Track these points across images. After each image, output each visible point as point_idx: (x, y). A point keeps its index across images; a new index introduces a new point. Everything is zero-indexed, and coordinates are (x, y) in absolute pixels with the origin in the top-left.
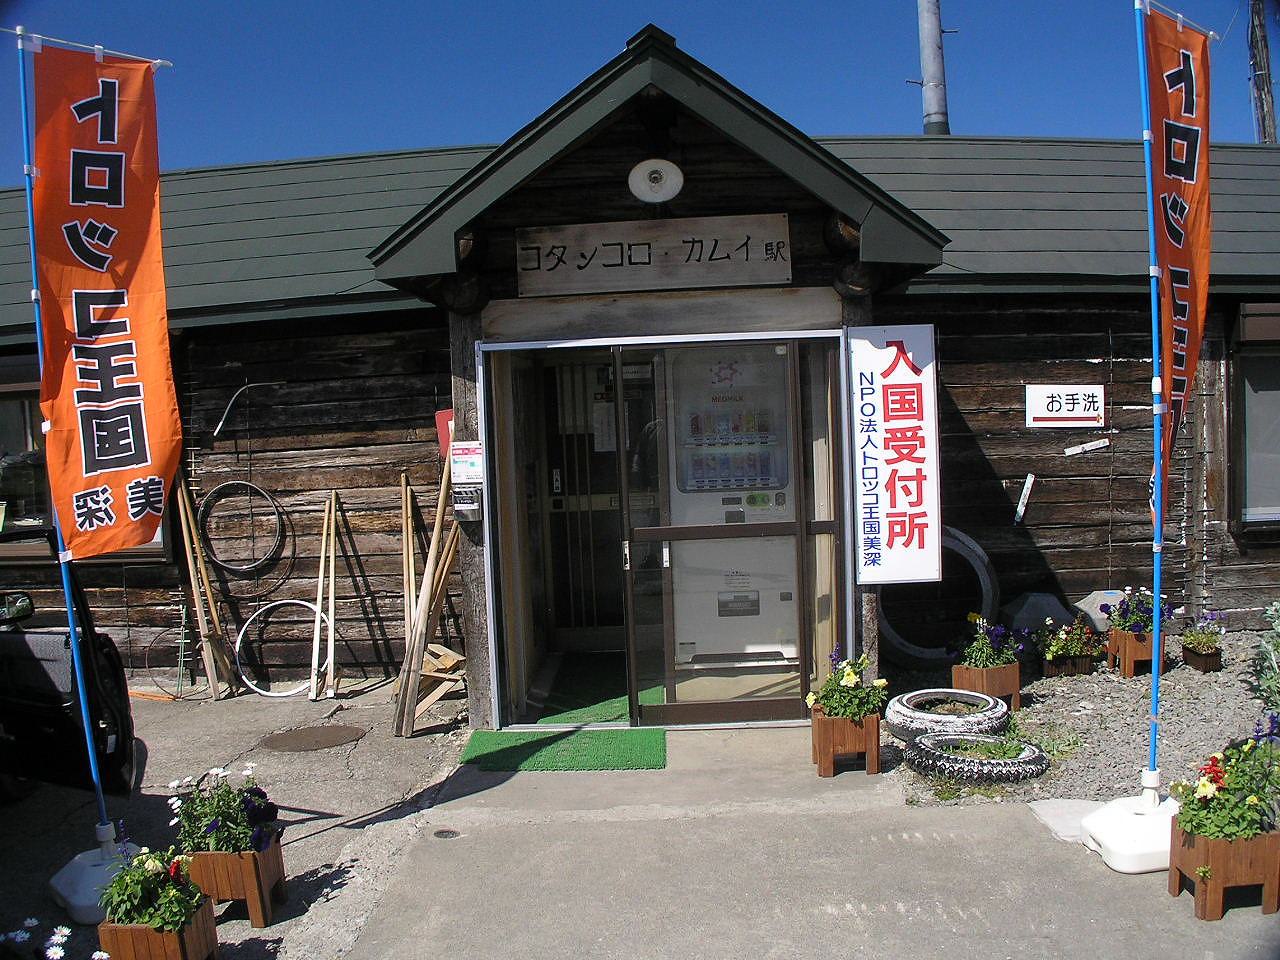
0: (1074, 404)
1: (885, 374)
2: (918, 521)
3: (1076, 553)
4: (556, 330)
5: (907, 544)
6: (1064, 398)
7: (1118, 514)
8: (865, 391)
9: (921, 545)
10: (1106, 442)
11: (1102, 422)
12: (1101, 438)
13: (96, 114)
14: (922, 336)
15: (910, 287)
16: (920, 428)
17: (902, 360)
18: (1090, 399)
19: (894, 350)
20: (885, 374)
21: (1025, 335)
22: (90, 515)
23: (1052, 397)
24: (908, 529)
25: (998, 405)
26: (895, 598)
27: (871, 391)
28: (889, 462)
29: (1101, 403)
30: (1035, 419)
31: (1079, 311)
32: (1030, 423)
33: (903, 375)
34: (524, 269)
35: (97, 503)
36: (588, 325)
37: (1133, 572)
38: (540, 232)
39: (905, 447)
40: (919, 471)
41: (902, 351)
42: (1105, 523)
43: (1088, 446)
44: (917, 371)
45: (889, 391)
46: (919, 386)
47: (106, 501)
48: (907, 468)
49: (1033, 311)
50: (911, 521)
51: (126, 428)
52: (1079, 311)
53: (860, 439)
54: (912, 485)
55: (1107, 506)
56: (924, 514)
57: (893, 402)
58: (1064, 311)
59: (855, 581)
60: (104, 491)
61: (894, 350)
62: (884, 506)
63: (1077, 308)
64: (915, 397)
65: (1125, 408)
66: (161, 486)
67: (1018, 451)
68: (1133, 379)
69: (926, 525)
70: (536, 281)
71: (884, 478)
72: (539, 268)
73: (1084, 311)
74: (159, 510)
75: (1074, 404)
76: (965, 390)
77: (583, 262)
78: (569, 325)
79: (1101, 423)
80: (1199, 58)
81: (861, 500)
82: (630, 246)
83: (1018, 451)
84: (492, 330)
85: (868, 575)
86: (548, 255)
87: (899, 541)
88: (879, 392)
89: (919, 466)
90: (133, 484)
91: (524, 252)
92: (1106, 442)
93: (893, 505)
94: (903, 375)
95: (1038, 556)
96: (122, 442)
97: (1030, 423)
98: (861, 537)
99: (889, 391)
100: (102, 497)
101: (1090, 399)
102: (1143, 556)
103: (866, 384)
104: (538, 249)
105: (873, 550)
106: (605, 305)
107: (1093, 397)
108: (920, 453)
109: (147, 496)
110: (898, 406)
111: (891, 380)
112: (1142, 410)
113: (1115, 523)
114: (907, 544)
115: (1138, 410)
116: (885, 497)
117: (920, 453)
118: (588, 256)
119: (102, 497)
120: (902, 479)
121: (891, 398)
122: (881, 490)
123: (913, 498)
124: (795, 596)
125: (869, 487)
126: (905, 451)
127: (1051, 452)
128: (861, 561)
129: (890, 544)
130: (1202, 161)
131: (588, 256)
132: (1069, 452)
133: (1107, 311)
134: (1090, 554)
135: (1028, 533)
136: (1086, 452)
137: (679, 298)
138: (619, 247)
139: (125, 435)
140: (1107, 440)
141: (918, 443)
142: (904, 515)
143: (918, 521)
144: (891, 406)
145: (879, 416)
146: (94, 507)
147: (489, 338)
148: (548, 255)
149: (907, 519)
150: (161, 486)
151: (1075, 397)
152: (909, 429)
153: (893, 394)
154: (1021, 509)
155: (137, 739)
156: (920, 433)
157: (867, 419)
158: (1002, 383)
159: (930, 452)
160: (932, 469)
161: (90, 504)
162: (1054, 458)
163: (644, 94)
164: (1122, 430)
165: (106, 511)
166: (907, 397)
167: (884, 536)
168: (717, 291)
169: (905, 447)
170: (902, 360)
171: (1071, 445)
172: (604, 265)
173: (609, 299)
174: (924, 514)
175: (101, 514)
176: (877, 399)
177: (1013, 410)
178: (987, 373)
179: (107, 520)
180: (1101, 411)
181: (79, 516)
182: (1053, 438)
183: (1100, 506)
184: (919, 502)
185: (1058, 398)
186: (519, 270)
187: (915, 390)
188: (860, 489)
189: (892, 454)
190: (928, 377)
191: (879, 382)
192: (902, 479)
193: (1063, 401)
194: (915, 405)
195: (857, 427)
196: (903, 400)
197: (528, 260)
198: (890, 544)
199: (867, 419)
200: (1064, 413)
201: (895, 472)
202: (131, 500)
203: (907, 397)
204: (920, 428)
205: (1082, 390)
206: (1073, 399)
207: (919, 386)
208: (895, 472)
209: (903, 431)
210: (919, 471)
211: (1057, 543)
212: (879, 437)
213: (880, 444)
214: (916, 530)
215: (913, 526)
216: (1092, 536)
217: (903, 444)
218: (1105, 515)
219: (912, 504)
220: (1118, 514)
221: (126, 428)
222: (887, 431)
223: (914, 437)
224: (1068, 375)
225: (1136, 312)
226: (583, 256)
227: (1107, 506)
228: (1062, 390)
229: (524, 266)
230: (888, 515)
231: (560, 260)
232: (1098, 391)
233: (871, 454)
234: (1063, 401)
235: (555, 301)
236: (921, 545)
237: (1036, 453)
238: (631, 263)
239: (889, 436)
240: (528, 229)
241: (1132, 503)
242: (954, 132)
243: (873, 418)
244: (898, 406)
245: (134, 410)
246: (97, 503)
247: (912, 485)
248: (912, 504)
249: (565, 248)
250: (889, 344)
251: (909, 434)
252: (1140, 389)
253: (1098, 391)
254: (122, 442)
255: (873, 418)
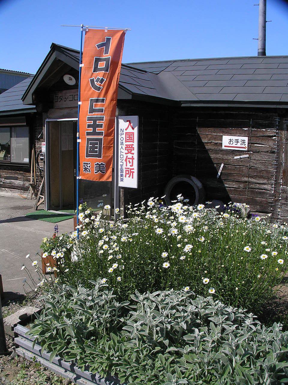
0: (237, 142)
1: (126, 130)
2: (132, 171)
3: (236, 190)
5: (129, 177)
6: (234, 140)
7: (250, 179)
8: (122, 134)
9: (133, 178)
10: (248, 156)
11: (247, 149)
12: (246, 154)
13: (104, 62)
14: (135, 118)
15: (182, 104)
16: (133, 145)
17: (130, 126)
18: (243, 141)
19: (128, 123)
20: (126, 130)
21: (223, 120)
22: (86, 169)
23: (231, 140)
24: (130, 172)
25: (213, 141)
26: (127, 190)
27: (123, 134)
28: (126, 154)
29: (247, 143)
30: (225, 146)
31: (242, 113)
32: (223, 148)
33: (130, 130)
35: (88, 166)
37: (254, 199)
39: (130, 150)
40: (133, 157)
41: (130, 123)
42: (246, 182)
43: (242, 157)
44: (133, 129)
46: (133, 133)
47: (89, 167)
48: (130, 156)
49: (227, 112)
50: (130, 171)
51: (97, 146)
52: (242, 113)
53: (120, 147)
54: (131, 160)
55: (247, 176)
56: (133, 169)
57: (128, 137)
58: (237, 112)
60: (89, 164)
61: (128, 123)
62: (124, 166)
63: (241, 112)
64: (132, 136)
65: (255, 145)
67: (220, 156)
68: (258, 136)
69: (134, 172)
70: (58, 104)
71: (125, 158)
73: (244, 113)
75: (237, 142)
76: (204, 136)
77: (65, 100)
79: (246, 149)
81: (120, 163)
82: (74, 95)
83: (220, 156)
84: (50, 116)
85: (121, 184)
87: (128, 175)
88: (125, 134)
89: (133, 155)
92: (248, 156)
93: (126, 166)
94: (130, 130)
95: (224, 189)
96: (95, 150)
97: (223, 148)
98: (119, 174)
100: (88, 165)
101: (243, 141)
102: (258, 194)
103: (122, 132)
104: (58, 97)
105: (122, 177)
107: (244, 140)
108: (133, 152)
110: (128, 138)
111: (127, 131)
112: (261, 146)
113: (249, 182)
114: (129, 177)
115: (260, 146)
116: (125, 163)
117: (133, 152)
118: (67, 98)
119: (88, 165)
120: (129, 158)
121: (127, 136)
122: (124, 161)
123: (131, 164)
125: (122, 160)
126: (130, 151)
127: (230, 157)
128: (119, 180)
129: (126, 176)
130: (111, 66)
132: (236, 158)
133: (251, 113)
134: (240, 191)
135: (223, 182)
136: (241, 158)
138: (72, 96)
139: (96, 148)
140: (248, 155)
141: (132, 149)
142: (129, 168)
143: (132, 171)
144: (127, 138)
145: (124, 141)
146: (87, 167)
147: (49, 118)
149: (129, 170)
151: (238, 140)
152: (131, 145)
153: (128, 135)
154: (219, 174)
156: (133, 146)
157: (122, 141)
158: (215, 134)
159: (135, 151)
160: (136, 156)
161: (86, 166)
162: (230, 159)
164: (254, 152)
166: (131, 136)
167: (124, 174)
169: (130, 150)
170: (130, 126)
171: (236, 155)
172: (70, 101)
173: (71, 108)
174: (133, 169)
175: (88, 170)
176: (124, 136)
177: (218, 143)
178: (211, 131)
179: (89, 172)
180: (247, 146)
182: (231, 153)
183: (245, 176)
184: (132, 166)
185: (232, 140)
186: (54, 102)
188: (120, 161)
189: (127, 152)
190: (136, 131)
191: (125, 131)
192: (129, 158)
193: (234, 141)
194: (132, 138)
195: (120, 144)
196: (129, 137)
198: (126, 176)
199: (122, 141)
200: (234, 145)
201: (127, 156)
203: (131, 136)
204: (133, 145)
205: (240, 138)
206: (237, 141)
207: (133, 133)
208: (127, 156)
209: (129, 145)
210: (133, 157)
211: (231, 186)
212: (124, 147)
213: (124, 148)
214: (131, 173)
215: (131, 172)
216: (242, 186)
217: (129, 149)
218: (246, 179)
219: (131, 166)
220: (250, 179)
221: (97, 146)
222: (126, 145)
223: (132, 147)
224: (236, 133)
225: (261, 114)
226: (66, 98)
227: (247, 176)
228: (234, 138)
230: (125, 168)
232: (246, 139)
233: (122, 151)
234: (234, 141)
235: (61, 109)
236: (133, 178)
237: (225, 157)
238: (74, 100)
239: (126, 146)
241: (255, 177)
242: (268, 54)
243: (123, 141)
244: (128, 138)
246: (88, 166)
247: (131, 160)
248: (131, 166)
250: (127, 121)
251: (131, 146)
252: (261, 139)
253: (246, 139)
254: (95, 150)
255: (123, 141)
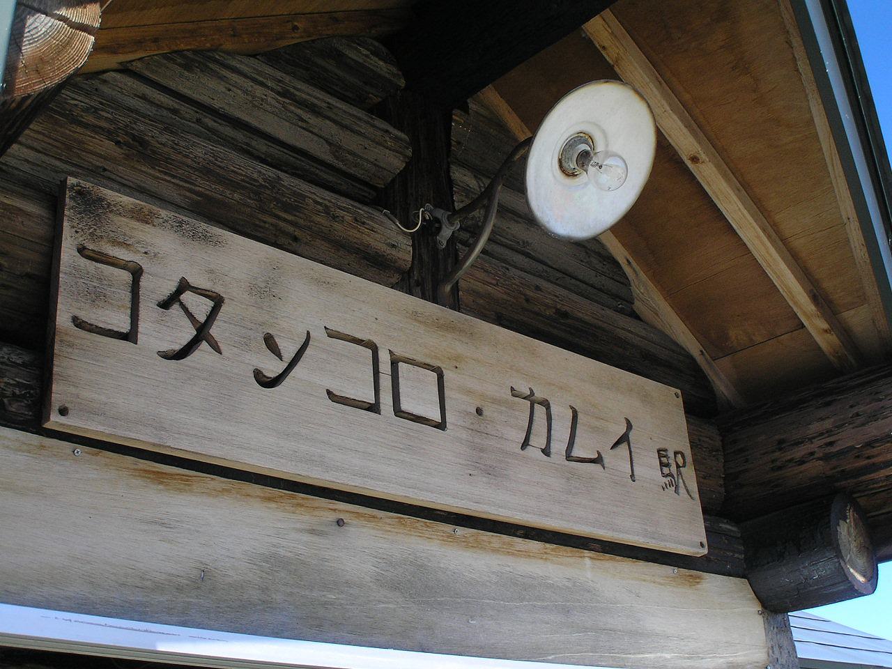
4: (158, 587)
34: (78, 323)
36: (264, 590)
38: (144, 218)
72: (130, 336)
77: (273, 368)
78: (203, 578)
86: (165, 305)
91: (84, 262)
106: (312, 532)
124: (689, 164)
131: (289, 350)
137: (495, 551)
148: (165, 305)
163: (526, 149)
168: (422, 522)
173: (327, 510)
186: (63, 319)
197: (97, 297)
226: (270, 343)
229: (84, 315)
231: (202, 333)
240: (110, 194)
249: (441, 426)
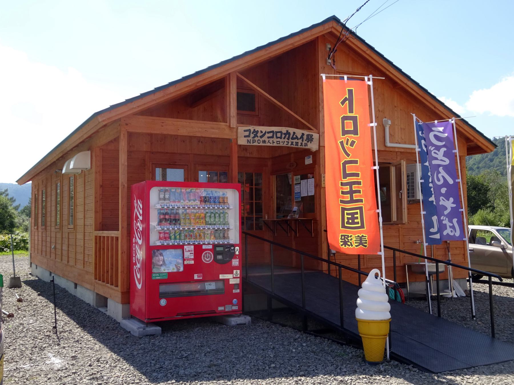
45: (346, 212)
59: (493, 276)
66: (366, 238)
74: (366, 246)
80: (505, 279)
90: (357, 236)
99: (346, 212)
109: (361, 240)
139: (357, 218)
150: (366, 238)
153: (358, 223)
155: (343, 280)
165: (351, 243)
181: (341, 242)
187: (358, 211)
202: (355, 241)
245: (360, 209)
